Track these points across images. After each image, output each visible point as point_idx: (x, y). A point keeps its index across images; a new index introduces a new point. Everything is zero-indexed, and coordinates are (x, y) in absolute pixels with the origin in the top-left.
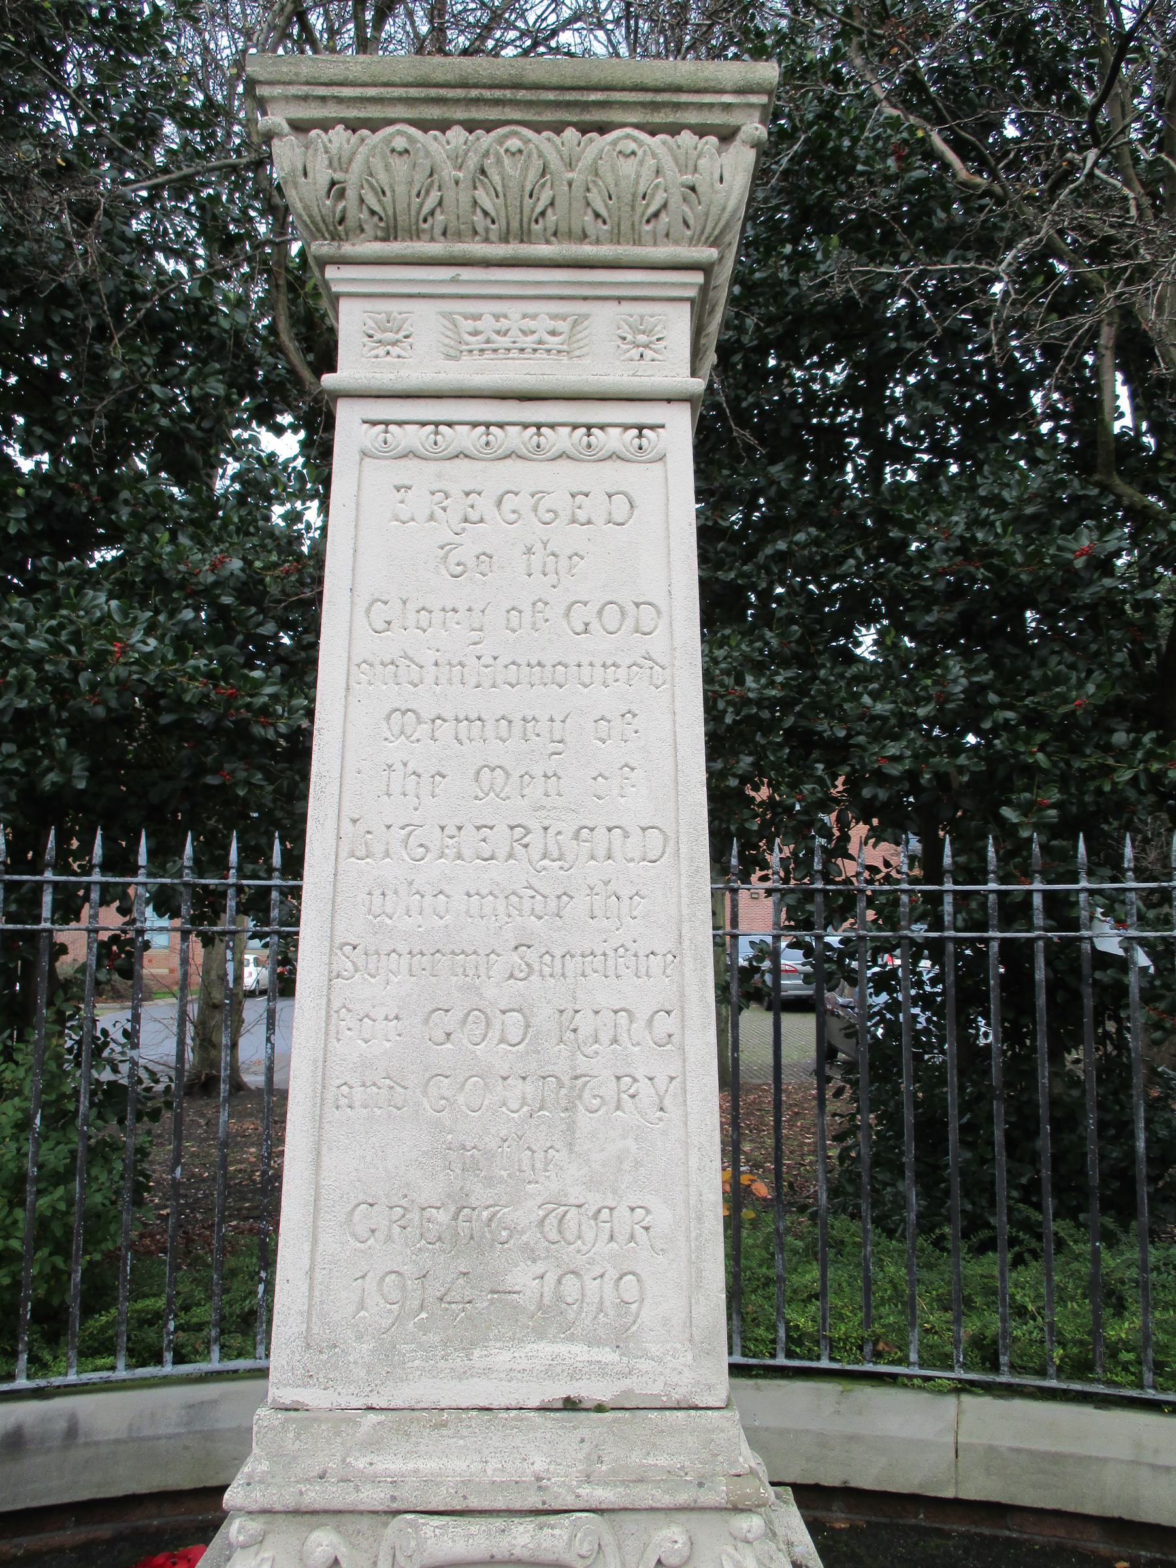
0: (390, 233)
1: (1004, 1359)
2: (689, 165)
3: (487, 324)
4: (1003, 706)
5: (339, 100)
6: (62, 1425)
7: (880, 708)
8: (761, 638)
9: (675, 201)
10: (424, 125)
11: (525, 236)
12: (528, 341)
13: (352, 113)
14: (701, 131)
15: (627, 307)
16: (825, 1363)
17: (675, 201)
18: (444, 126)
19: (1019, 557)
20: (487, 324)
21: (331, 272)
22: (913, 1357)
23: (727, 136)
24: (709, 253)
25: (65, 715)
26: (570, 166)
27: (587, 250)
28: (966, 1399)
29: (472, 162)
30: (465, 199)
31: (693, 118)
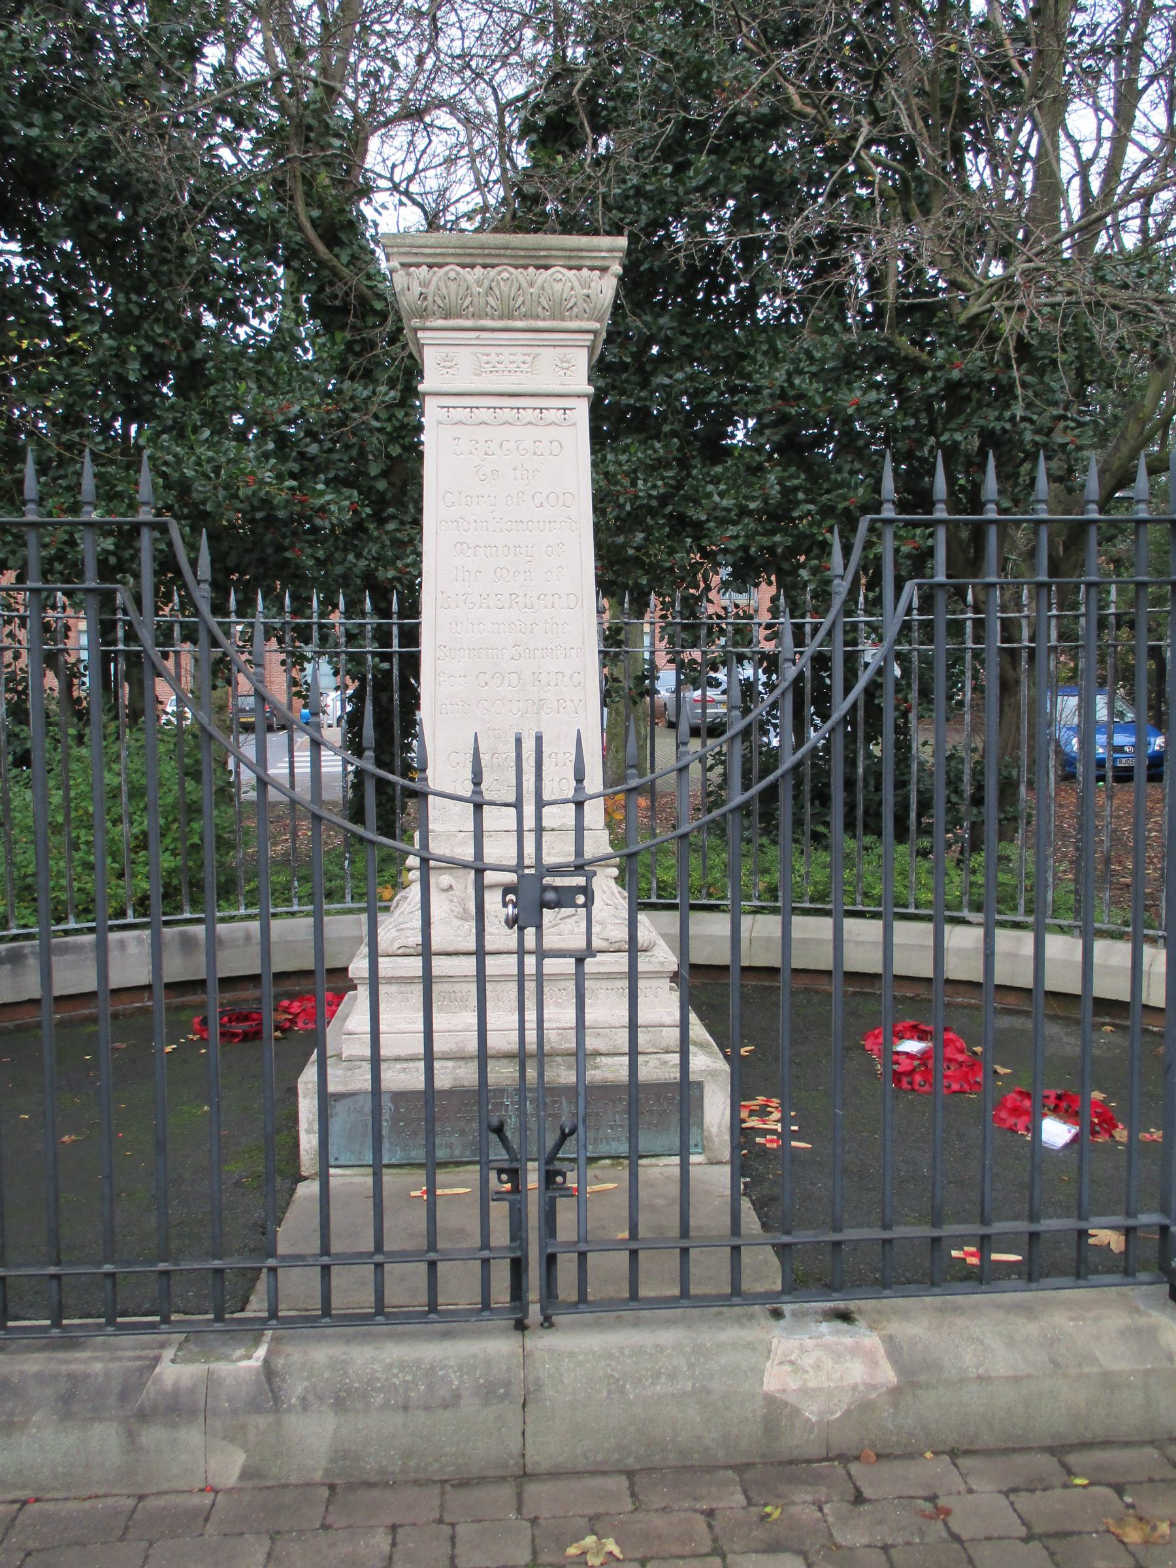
2: (585, 285)
3: (493, 358)
4: (807, 501)
5: (423, 254)
6: (241, 934)
7: (726, 502)
8: (652, 447)
9: (580, 302)
10: (463, 266)
11: (510, 317)
12: (513, 367)
14: (592, 269)
15: (558, 350)
17: (580, 302)
18: (472, 266)
19: (819, 401)
20: (493, 358)
21: (420, 334)
23: (604, 270)
24: (596, 325)
25: (186, 511)
27: (540, 324)
28: (759, 917)
29: (486, 283)
30: (483, 301)
31: (588, 263)
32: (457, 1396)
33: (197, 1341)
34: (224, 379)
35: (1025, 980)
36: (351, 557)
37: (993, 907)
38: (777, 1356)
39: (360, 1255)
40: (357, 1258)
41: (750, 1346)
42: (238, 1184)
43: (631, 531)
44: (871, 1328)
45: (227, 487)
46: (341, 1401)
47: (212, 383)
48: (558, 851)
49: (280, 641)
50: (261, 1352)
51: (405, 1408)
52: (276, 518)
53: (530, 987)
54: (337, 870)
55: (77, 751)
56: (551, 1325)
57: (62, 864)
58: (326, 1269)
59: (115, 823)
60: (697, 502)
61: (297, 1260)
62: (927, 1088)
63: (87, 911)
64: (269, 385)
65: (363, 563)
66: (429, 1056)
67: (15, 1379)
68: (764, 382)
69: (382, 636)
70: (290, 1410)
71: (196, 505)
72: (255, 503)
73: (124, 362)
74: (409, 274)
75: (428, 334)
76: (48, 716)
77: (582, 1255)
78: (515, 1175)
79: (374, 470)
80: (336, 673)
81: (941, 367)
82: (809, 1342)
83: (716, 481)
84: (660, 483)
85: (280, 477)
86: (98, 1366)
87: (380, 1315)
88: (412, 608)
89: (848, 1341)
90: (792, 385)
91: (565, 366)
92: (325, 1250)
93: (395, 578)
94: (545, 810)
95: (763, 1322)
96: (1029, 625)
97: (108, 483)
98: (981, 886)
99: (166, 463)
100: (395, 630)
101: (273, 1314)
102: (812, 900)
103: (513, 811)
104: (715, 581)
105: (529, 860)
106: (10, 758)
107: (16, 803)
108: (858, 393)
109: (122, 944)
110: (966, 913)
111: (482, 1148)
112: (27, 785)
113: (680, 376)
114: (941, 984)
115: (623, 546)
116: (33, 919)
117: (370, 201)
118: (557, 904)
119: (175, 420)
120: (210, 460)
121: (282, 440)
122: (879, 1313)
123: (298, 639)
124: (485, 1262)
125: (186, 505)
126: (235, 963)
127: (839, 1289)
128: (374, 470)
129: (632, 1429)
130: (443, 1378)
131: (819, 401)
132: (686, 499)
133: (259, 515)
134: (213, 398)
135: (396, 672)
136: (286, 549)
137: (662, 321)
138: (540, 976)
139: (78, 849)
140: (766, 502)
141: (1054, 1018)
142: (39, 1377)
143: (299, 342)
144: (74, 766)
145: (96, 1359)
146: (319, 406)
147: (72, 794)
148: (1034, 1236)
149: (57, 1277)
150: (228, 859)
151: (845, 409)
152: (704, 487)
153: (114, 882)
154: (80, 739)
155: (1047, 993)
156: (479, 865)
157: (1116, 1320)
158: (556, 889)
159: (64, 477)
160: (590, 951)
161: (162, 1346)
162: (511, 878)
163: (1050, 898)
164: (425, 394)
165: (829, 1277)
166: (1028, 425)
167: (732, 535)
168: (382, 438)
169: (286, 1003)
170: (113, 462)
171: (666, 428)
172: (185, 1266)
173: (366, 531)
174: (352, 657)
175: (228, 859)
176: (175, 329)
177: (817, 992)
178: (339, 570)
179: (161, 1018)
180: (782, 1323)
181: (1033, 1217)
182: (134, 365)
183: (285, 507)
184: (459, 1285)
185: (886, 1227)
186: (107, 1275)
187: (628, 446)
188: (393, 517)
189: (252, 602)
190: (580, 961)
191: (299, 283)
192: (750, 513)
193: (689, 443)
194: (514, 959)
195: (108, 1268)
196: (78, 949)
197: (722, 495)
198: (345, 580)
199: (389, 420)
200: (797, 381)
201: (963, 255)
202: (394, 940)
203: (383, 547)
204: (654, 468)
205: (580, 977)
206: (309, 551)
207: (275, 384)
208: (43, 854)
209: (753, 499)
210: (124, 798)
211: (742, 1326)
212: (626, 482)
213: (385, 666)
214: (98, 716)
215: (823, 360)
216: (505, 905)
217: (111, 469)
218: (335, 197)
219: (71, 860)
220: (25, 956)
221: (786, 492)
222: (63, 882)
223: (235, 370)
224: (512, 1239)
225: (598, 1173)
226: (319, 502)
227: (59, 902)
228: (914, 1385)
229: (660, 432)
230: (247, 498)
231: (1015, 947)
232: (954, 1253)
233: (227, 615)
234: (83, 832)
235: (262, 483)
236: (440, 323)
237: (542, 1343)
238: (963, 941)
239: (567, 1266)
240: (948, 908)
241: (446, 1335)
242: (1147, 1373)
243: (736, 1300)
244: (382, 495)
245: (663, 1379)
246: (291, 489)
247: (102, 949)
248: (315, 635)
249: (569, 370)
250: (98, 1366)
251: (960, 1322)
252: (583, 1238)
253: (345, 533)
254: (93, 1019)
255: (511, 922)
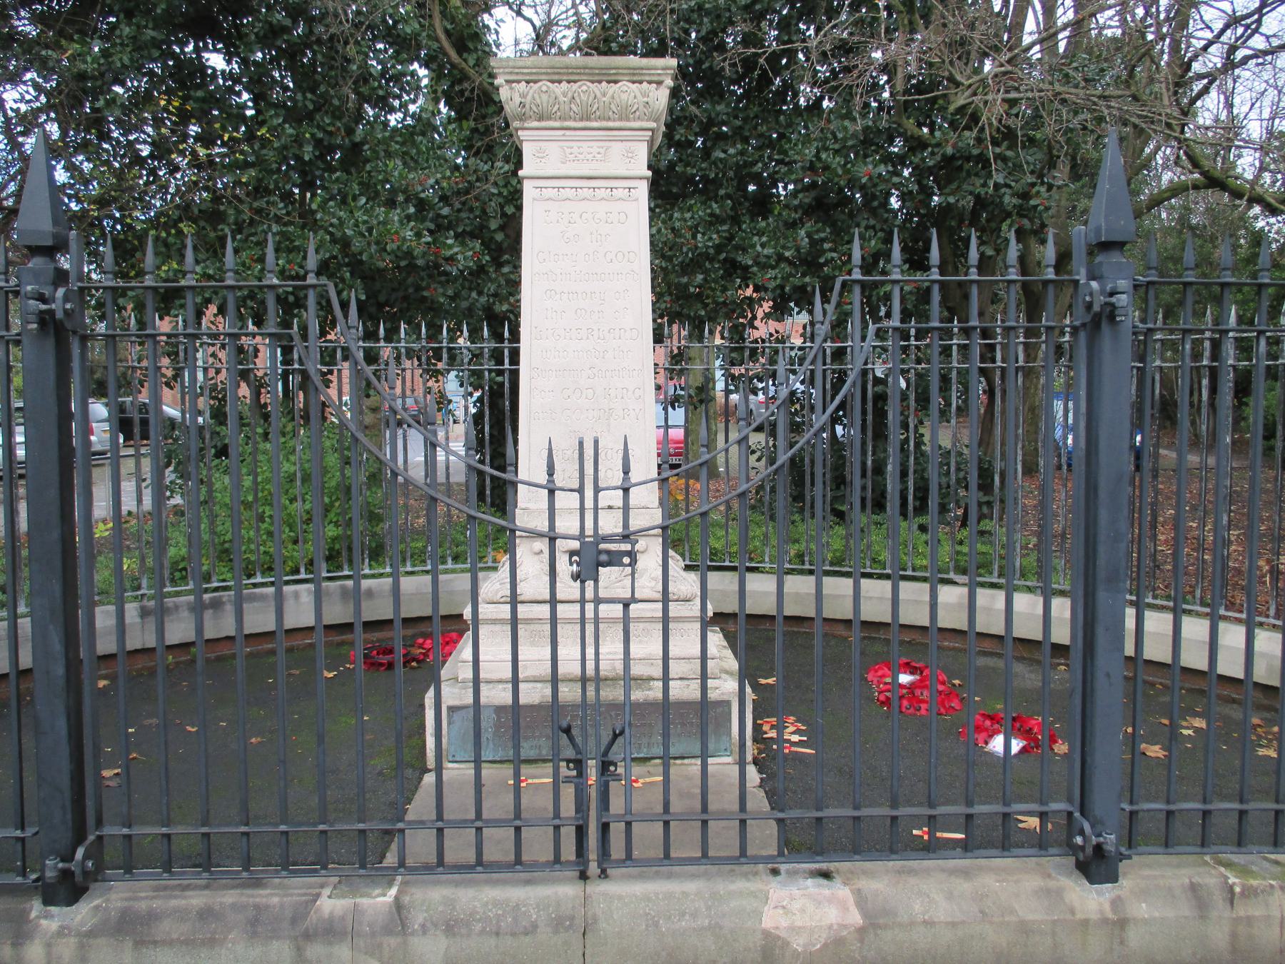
0: (540, 119)
1: (806, 559)
2: (645, 95)
3: (575, 150)
4: (831, 250)
8: (710, 207)
9: (641, 107)
10: (553, 82)
11: (588, 119)
12: (590, 157)
13: (527, 78)
14: (650, 82)
16: (727, 563)
17: (641, 107)
18: (560, 82)
19: (840, 172)
20: (575, 150)
21: (520, 133)
22: (767, 559)
23: (659, 83)
24: (654, 125)
26: (604, 95)
27: (611, 124)
29: (570, 95)
30: (567, 108)
31: (647, 78)
32: (535, 926)
33: (347, 885)
34: (377, 158)
35: (999, 629)
36: (474, 295)
37: (974, 571)
38: (771, 903)
39: (465, 821)
40: (462, 824)
41: (753, 895)
42: (380, 773)
43: (693, 273)
44: (845, 884)
45: (377, 243)
46: (451, 927)
47: (368, 161)
48: (610, 524)
49: (419, 359)
50: (393, 891)
51: (497, 934)
52: (416, 266)
53: (589, 627)
54: (462, 538)
55: (262, 446)
56: (606, 877)
57: (252, 533)
58: (440, 830)
59: (292, 500)
60: (744, 250)
61: (420, 824)
62: (912, 711)
63: (270, 569)
64: (411, 162)
65: (483, 299)
66: (515, 681)
67: (217, 908)
68: (797, 157)
69: (497, 356)
70: (412, 934)
71: (354, 255)
72: (399, 254)
73: (301, 146)
74: (511, 89)
75: (526, 133)
76: (241, 418)
77: (628, 824)
78: (579, 764)
79: (494, 225)
80: (461, 385)
81: (938, 145)
82: (796, 892)
83: (760, 233)
84: (715, 236)
85: (418, 235)
86: (276, 900)
87: (480, 865)
88: (515, 336)
89: (827, 892)
90: (819, 159)
91: (630, 155)
92: (440, 817)
93: (508, 311)
94: (601, 494)
95: (764, 877)
96: (1002, 350)
97: (288, 239)
98: (965, 554)
99: (332, 225)
100: (506, 352)
101: (402, 864)
102: (832, 564)
103: (576, 495)
104: (760, 314)
105: (589, 530)
106: (213, 451)
107: (218, 485)
108: (870, 167)
109: (297, 595)
110: (952, 575)
111: (556, 749)
112: (225, 472)
113: (732, 151)
114: (973, 636)
115: (686, 286)
116: (229, 575)
117: (491, 15)
118: (609, 564)
119: (339, 190)
120: (365, 222)
121: (422, 205)
122: (852, 873)
123: (433, 362)
124: (557, 828)
125: (347, 256)
126: (381, 610)
127: (821, 853)
128: (494, 225)
129: (664, 953)
130: (525, 913)
131: (840, 172)
132: (737, 248)
133: (403, 263)
134: (369, 172)
135: (507, 385)
136: (424, 289)
137: (719, 108)
138: (597, 620)
139: (264, 522)
140: (798, 250)
141: (1020, 659)
142: (233, 906)
143: (435, 129)
144: (261, 457)
145: (272, 895)
146: (449, 178)
147: (259, 479)
148: (969, 817)
149: (247, 834)
150: (378, 529)
151: (860, 178)
152: (751, 239)
153: (290, 546)
154: (266, 436)
155: (1015, 639)
156: (552, 534)
157: (1032, 882)
158: (608, 552)
159: (255, 234)
160: (633, 600)
161: (322, 886)
162: (575, 545)
163: (1018, 564)
164: (524, 178)
165: (812, 842)
166: (1008, 191)
167: (771, 277)
168: (501, 200)
169: (421, 641)
170: (291, 223)
171: (722, 192)
172: (338, 827)
173: (487, 273)
174: (473, 373)
175: (378, 529)
176: (340, 118)
177: (834, 636)
178: (465, 304)
179: (321, 650)
180: (778, 878)
181: (969, 803)
182: (308, 149)
183: (423, 257)
184: (538, 844)
185: (856, 808)
186: (282, 832)
187: (691, 206)
188: (508, 262)
189: (397, 330)
190: (626, 606)
191: (437, 77)
192: (787, 259)
193: (740, 204)
194: (578, 606)
195: (283, 828)
196: (263, 598)
197: (763, 246)
198: (470, 312)
199: (505, 186)
200: (824, 156)
201: (947, 61)
202: (497, 591)
203: (499, 286)
204: (715, 220)
205: (626, 620)
206: (441, 290)
207: (416, 162)
208: (237, 524)
209: (788, 249)
210: (299, 483)
211: (748, 880)
212: (689, 236)
213: (499, 379)
214: (278, 421)
215: (845, 139)
216: (571, 564)
217: (291, 229)
218: (465, 16)
219: (258, 529)
220: (223, 603)
221: (813, 243)
222: (252, 547)
223: (386, 151)
224: (577, 812)
225: (651, 769)
226: (449, 253)
227: (249, 561)
228: (875, 926)
229: (717, 195)
230: (393, 251)
231: (991, 601)
232: (915, 832)
233: (378, 340)
234: (267, 508)
235: (404, 239)
236: (535, 124)
237: (598, 889)
238: (951, 596)
239: (617, 829)
240: (939, 571)
241: (528, 882)
242: (1054, 922)
243: (743, 860)
244: (499, 245)
245: (687, 917)
246: (428, 243)
247: (279, 599)
248: (445, 356)
249: (632, 158)
250: (276, 900)
251: (912, 881)
252: (628, 811)
253: (470, 274)
254: (273, 652)
255: (576, 577)
